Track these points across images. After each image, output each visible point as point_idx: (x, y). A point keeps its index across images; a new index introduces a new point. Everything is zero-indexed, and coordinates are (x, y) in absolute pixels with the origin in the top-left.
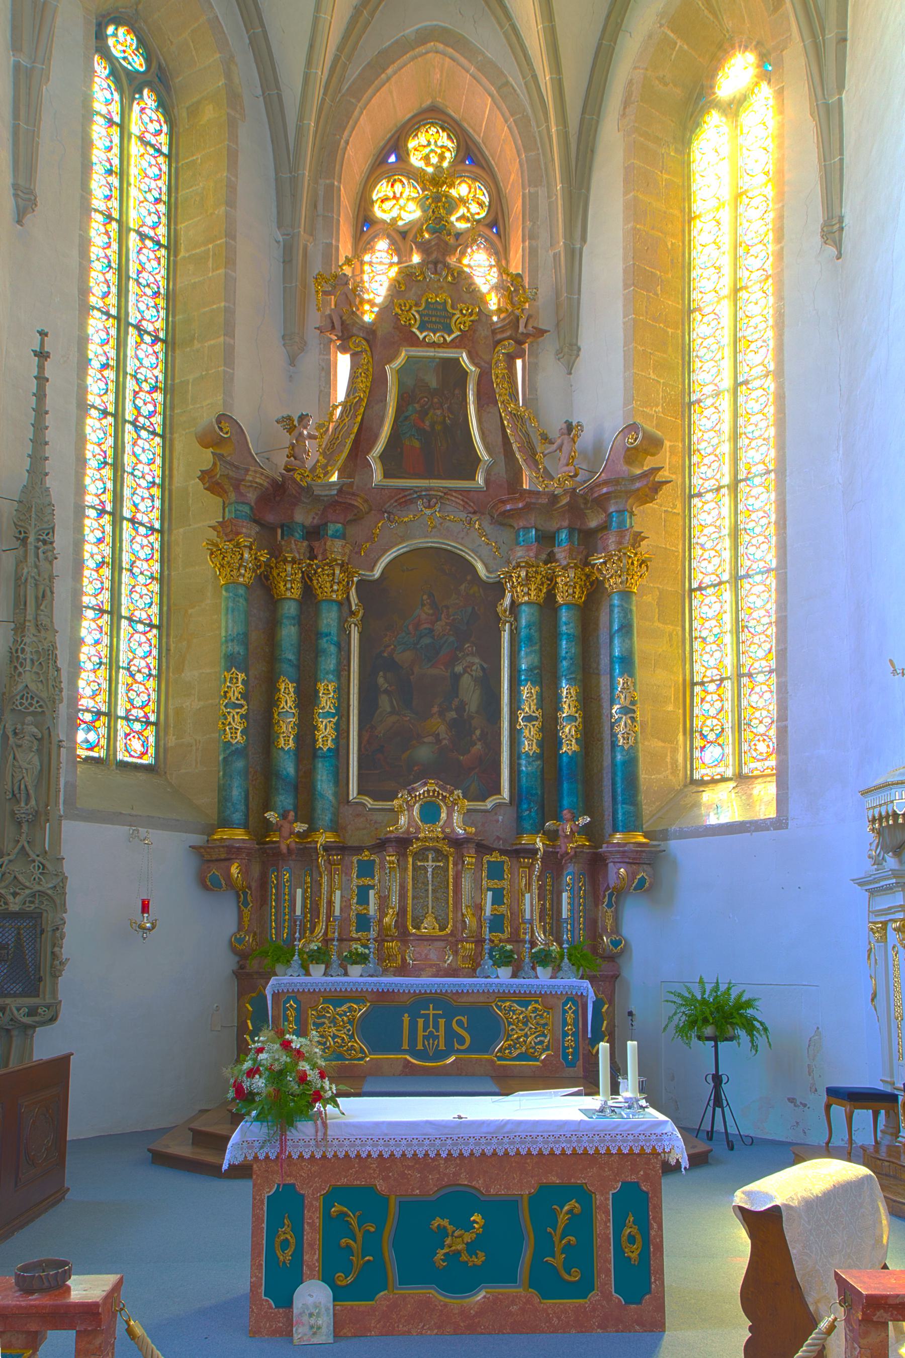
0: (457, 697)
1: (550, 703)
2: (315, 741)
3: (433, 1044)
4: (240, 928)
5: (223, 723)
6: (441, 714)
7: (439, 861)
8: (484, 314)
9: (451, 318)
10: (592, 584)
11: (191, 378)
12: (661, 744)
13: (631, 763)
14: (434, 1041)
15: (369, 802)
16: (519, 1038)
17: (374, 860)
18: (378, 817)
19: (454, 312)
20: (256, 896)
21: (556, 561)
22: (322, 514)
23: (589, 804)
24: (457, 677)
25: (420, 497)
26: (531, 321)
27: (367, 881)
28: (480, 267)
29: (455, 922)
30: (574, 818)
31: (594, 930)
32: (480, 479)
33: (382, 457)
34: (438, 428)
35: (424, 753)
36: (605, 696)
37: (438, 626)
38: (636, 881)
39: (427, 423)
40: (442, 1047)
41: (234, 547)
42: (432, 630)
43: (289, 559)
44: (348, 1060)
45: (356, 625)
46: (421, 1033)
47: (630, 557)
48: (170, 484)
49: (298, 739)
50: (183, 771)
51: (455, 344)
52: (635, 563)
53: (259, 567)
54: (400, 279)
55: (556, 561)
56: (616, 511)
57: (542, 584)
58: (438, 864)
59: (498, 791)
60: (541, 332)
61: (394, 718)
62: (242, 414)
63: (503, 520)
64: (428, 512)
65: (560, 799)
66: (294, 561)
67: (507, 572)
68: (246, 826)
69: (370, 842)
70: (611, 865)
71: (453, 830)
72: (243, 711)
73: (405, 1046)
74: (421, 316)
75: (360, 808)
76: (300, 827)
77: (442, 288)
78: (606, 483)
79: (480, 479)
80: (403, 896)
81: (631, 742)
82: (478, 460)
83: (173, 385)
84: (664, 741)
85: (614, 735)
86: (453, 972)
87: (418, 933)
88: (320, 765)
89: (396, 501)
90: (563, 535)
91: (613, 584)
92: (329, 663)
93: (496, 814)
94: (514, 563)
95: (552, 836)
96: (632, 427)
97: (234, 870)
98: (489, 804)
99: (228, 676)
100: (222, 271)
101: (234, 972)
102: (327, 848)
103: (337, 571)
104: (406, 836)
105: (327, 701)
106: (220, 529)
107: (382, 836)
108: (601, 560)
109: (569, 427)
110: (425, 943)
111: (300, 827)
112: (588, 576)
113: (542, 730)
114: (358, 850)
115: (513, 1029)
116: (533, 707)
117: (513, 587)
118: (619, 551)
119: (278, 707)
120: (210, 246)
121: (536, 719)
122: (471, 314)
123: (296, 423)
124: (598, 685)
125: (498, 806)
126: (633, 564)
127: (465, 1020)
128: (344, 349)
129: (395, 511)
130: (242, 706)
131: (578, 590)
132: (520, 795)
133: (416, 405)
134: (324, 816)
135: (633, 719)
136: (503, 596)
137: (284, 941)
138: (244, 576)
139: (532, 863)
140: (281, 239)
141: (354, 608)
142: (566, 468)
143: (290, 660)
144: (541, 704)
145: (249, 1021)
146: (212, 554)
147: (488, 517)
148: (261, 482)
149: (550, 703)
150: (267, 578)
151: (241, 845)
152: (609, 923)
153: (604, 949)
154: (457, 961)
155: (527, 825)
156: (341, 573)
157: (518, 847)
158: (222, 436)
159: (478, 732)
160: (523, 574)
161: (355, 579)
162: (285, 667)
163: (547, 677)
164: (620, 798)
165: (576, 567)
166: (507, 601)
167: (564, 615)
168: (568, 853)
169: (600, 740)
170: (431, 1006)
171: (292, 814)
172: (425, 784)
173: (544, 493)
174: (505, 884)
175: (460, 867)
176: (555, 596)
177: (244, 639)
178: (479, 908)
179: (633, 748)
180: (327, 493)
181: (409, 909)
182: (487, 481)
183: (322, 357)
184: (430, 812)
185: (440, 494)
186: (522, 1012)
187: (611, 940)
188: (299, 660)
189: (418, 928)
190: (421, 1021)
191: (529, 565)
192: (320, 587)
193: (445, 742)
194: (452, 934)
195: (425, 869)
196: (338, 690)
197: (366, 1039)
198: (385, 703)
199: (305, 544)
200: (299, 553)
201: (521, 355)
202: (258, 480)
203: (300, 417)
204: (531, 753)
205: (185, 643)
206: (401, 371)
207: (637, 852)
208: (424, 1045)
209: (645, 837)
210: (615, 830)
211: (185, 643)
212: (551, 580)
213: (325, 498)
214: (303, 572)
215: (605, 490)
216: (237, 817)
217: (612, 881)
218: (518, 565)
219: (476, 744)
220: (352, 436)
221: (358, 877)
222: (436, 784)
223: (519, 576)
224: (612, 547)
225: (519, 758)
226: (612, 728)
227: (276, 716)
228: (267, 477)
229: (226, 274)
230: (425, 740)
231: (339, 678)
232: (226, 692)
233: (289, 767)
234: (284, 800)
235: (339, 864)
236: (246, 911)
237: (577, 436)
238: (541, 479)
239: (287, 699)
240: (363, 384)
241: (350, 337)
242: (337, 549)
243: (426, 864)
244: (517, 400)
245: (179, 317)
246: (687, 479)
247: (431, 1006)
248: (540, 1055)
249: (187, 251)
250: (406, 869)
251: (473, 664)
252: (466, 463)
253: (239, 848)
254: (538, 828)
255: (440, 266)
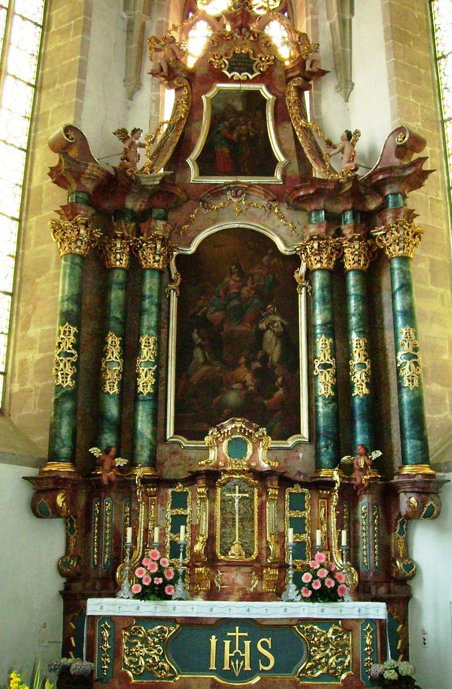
0: (261, 349)
1: (341, 352)
2: (137, 386)
3: (239, 665)
4: (67, 552)
5: (56, 370)
6: (248, 364)
7: (246, 493)
8: (277, 61)
9: (253, 63)
10: (374, 254)
11: (51, 109)
12: (439, 387)
13: (418, 402)
14: (240, 662)
15: (184, 441)
16: (321, 659)
17: (187, 492)
18: (192, 454)
19: (255, 59)
20: (81, 525)
21: (343, 236)
22: (148, 202)
23: (379, 436)
24: (261, 333)
25: (229, 189)
26: (315, 64)
27: (180, 511)
28: (276, 32)
29: (260, 549)
30: (367, 452)
31: (387, 555)
32: (278, 175)
33: (199, 161)
34: (244, 138)
35: (232, 398)
36: (390, 347)
37: (244, 291)
38: (426, 509)
39: (235, 135)
40: (247, 668)
41: (73, 224)
42: (239, 294)
43: (119, 235)
44: (158, 679)
45: (174, 290)
46: (227, 655)
47: (405, 229)
48: (29, 185)
49: (122, 384)
50: (23, 413)
51: (254, 81)
52: (410, 233)
53: (93, 242)
54: (214, 39)
55: (343, 236)
56: (391, 194)
57: (332, 254)
58: (244, 495)
59: (298, 431)
60: (323, 73)
61: (205, 368)
62: (88, 130)
63: (298, 204)
64: (235, 200)
65: (353, 437)
66: (123, 237)
67: (302, 246)
68: (72, 459)
69: (183, 475)
70: (402, 495)
71: (258, 464)
72: (74, 359)
73: (213, 667)
74: (229, 62)
75: (176, 446)
76: (121, 462)
77: (245, 44)
78: (382, 171)
79: (278, 175)
80: (212, 525)
81: (416, 383)
82: (275, 162)
83: (38, 115)
84: (443, 385)
85: (399, 378)
86: (257, 597)
87: (226, 560)
88: (140, 408)
89: (209, 192)
90: (348, 216)
91: (394, 251)
92: (149, 321)
93: (297, 451)
94: (308, 238)
95: (347, 470)
96: (400, 130)
97: (60, 500)
98: (290, 442)
99: (62, 329)
100: (80, 36)
101: (61, 593)
102: (144, 481)
103: (159, 246)
104: (216, 469)
105: (147, 353)
106: (63, 212)
107: (195, 469)
108: (382, 233)
109: (349, 135)
110: (233, 568)
111: (121, 462)
112: (370, 248)
113: (335, 376)
114: (172, 483)
115: (314, 651)
116: (328, 357)
117: (307, 257)
118: (397, 223)
119: (105, 358)
120: (73, 22)
121: (330, 366)
122: (268, 61)
123: (129, 135)
124: (383, 338)
125: (299, 444)
126: (408, 234)
127: (269, 642)
128: (170, 86)
129: (208, 200)
130: (72, 355)
131: (362, 258)
132: (318, 434)
133: (226, 123)
134: (144, 454)
135: (416, 364)
136: (299, 265)
137: (104, 565)
138: (80, 248)
139: (330, 494)
140: (125, 16)
141: (173, 276)
142: (348, 165)
143: (117, 318)
144: (333, 355)
145: (72, 638)
146: (55, 232)
147: (286, 205)
148: (98, 174)
149: (341, 352)
150: (101, 252)
151: (67, 476)
152: (401, 548)
153: (397, 573)
154: (262, 586)
155: (325, 460)
156: (162, 247)
157: (317, 479)
158: (71, 145)
159: (280, 380)
160: (316, 245)
161: (175, 253)
162: (113, 323)
163: (337, 329)
164: (408, 433)
165: (360, 239)
166: (303, 269)
167: (352, 279)
168: (363, 485)
169: (387, 385)
170: (237, 628)
171: (113, 450)
172: (233, 422)
173: (331, 181)
174: (306, 514)
175: (264, 498)
176: (343, 264)
177: (77, 299)
178: (282, 536)
179: (419, 389)
180: (151, 183)
181: (218, 537)
182: (284, 177)
183: (153, 93)
184: (237, 448)
185: (246, 186)
186: (323, 634)
187: (404, 565)
188: (125, 317)
189: (225, 553)
190: (227, 643)
191: (320, 238)
192: (145, 259)
193: (251, 388)
194: (258, 560)
195: (232, 499)
196: (158, 343)
197: (177, 659)
198: (198, 354)
199: (133, 225)
200: (128, 232)
201: (308, 88)
202: (95, 173)
203: (133, 131)
204: (327, 396)
205: (31, 306)
206: (212, 101)
207: (426, 482)
208: (230, 666)
209: (431, 468)
210: (404, 463)
211: (31, 306)
212: (340, 251)
213: (150, 188)
214: (130, 247)
215: (381, 177)
216: (65, 451)
217: (404, 508)
218: (311, 239)
219: (277, 390)
220: (175, 145)
221: (172, 508)
222: (243, 422)
223: (312, 247)
224: (390, 222)
225: (316, 400)
226: (398, 372)
227: (104, 366)
228: (103, 171)
229: (83, 39)
230: (235, 386)
231: (158, 333)
232: (60, 343)
233: (112, 409)
234: (109, 438)
235: (155, 496)
236: (72, 537)
237: (356, 141)
238: (328, 173)
239: (114, 352)
240: (183, 109)
241: (175, 77)
242: (159, 227)
243: (233, 495)
244: (306, 118)
245: (47, 70)
246: (445, 175)
247: (237, 628)
248: (341, 675)
249: (56, 27)
250: (213, 500)
251: (275, 322)
252: (267, 165)
253: (65, 480)
254: (336, 462)
255: (244, 30)
